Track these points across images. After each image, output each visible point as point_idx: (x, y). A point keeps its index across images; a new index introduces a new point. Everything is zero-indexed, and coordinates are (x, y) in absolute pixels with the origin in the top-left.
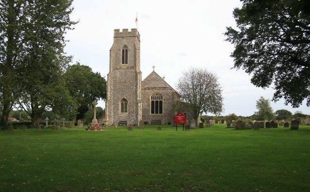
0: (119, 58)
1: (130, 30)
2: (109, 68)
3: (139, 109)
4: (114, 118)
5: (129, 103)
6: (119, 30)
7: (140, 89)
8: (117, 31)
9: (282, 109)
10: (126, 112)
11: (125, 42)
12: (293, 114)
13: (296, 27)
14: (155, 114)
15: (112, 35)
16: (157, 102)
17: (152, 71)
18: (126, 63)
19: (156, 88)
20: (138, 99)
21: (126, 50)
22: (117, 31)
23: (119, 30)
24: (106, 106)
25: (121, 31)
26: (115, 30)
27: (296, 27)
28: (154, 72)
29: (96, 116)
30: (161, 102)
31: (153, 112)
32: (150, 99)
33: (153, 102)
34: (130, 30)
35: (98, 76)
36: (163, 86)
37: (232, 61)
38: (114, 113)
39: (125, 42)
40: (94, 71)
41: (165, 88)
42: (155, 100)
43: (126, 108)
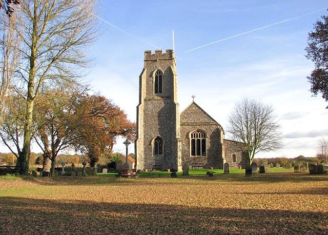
0: (139, 147)
2: (139, 92)
3: (178, 150)
5: (164, 142)
6: (150, 52)
7: (179, 125)
8: (148, 53)
9: (276, 157)
10: (161, 153)
14: (196, 156)
15: (143, 57)
17: (192, 102)
20: (177, 137)
22: (148, 53)
23: (150, 52)
24: (138, 119)
25: (153, 53)
26: (146, 52)
28: (194, 103)
31: (193, 154)
32: (190, 136)
33: (193, 141)
34: (164, 52)
37: (310, 85)
43: (161, 148)
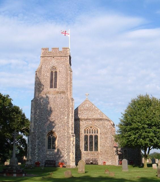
1: (61, 50)
4: (38, 156)
6: (47, 49)
11: (54, 62)
12: (5, 165)
13: (2, 154)
16: (91, 137)
18: (56, 87)
19: (89, 119)
21: (56, 72)
27: (2, 154)
29: (88, 137)
30: (96, 137)
35: (17, 111)
36: (99, 117)
38: (39, 150)
39: (54, 62)
40: (15, 103)
41: (101, 119)
42: (89, 135)
